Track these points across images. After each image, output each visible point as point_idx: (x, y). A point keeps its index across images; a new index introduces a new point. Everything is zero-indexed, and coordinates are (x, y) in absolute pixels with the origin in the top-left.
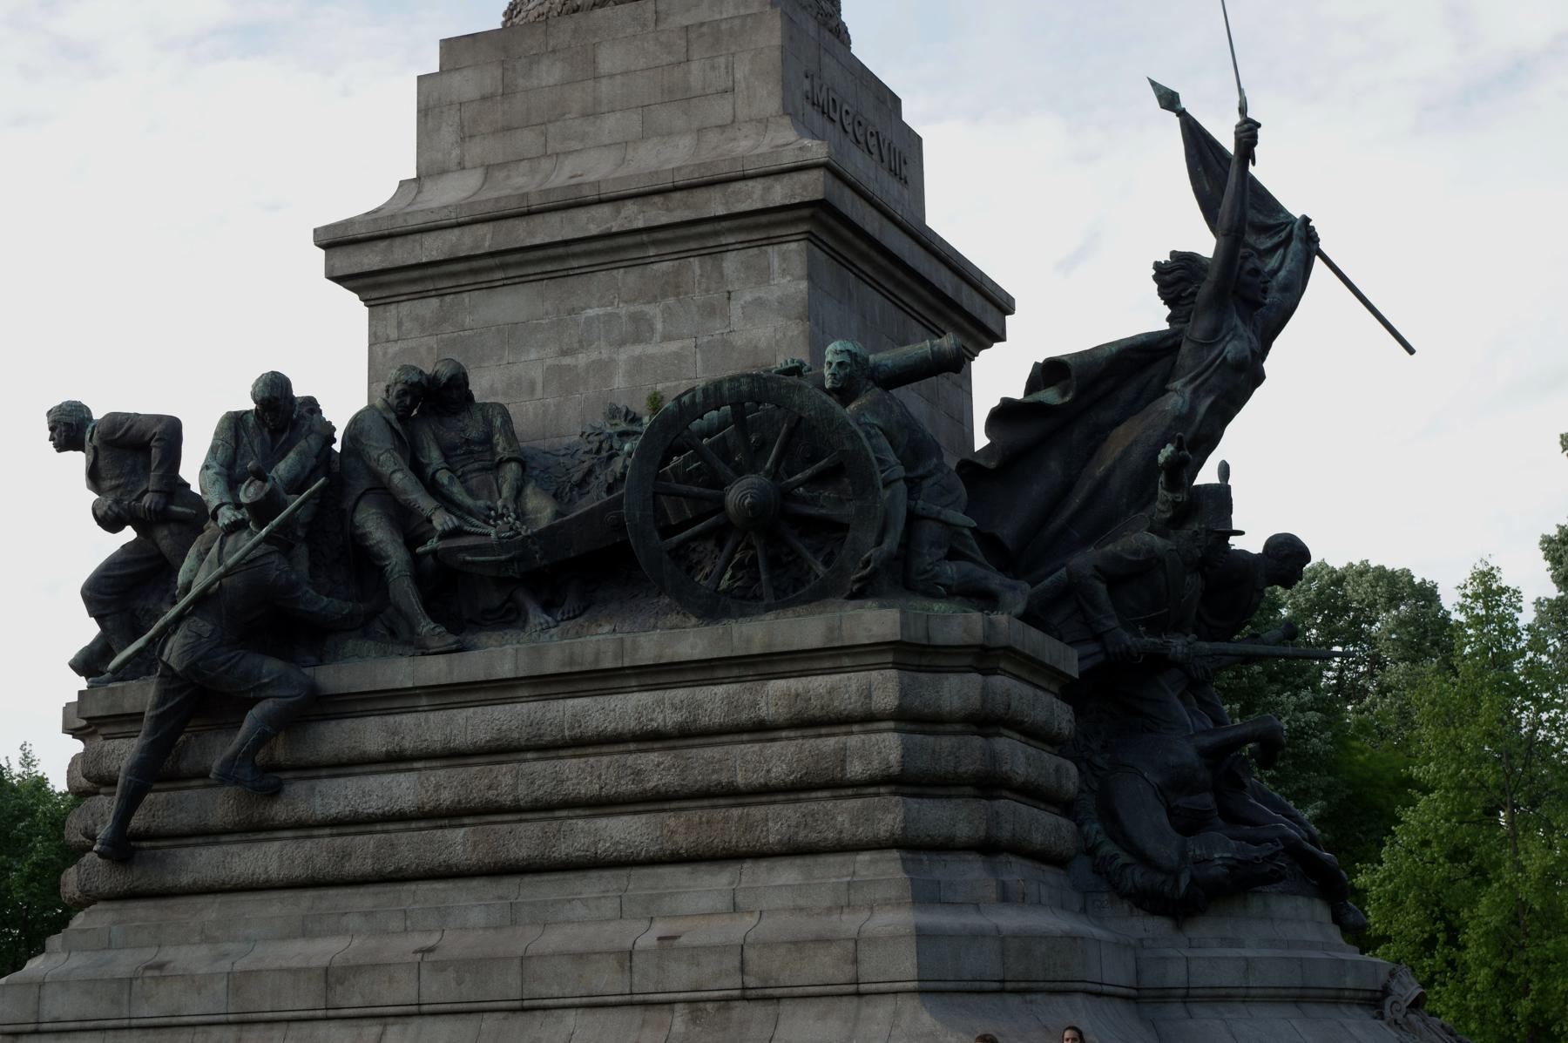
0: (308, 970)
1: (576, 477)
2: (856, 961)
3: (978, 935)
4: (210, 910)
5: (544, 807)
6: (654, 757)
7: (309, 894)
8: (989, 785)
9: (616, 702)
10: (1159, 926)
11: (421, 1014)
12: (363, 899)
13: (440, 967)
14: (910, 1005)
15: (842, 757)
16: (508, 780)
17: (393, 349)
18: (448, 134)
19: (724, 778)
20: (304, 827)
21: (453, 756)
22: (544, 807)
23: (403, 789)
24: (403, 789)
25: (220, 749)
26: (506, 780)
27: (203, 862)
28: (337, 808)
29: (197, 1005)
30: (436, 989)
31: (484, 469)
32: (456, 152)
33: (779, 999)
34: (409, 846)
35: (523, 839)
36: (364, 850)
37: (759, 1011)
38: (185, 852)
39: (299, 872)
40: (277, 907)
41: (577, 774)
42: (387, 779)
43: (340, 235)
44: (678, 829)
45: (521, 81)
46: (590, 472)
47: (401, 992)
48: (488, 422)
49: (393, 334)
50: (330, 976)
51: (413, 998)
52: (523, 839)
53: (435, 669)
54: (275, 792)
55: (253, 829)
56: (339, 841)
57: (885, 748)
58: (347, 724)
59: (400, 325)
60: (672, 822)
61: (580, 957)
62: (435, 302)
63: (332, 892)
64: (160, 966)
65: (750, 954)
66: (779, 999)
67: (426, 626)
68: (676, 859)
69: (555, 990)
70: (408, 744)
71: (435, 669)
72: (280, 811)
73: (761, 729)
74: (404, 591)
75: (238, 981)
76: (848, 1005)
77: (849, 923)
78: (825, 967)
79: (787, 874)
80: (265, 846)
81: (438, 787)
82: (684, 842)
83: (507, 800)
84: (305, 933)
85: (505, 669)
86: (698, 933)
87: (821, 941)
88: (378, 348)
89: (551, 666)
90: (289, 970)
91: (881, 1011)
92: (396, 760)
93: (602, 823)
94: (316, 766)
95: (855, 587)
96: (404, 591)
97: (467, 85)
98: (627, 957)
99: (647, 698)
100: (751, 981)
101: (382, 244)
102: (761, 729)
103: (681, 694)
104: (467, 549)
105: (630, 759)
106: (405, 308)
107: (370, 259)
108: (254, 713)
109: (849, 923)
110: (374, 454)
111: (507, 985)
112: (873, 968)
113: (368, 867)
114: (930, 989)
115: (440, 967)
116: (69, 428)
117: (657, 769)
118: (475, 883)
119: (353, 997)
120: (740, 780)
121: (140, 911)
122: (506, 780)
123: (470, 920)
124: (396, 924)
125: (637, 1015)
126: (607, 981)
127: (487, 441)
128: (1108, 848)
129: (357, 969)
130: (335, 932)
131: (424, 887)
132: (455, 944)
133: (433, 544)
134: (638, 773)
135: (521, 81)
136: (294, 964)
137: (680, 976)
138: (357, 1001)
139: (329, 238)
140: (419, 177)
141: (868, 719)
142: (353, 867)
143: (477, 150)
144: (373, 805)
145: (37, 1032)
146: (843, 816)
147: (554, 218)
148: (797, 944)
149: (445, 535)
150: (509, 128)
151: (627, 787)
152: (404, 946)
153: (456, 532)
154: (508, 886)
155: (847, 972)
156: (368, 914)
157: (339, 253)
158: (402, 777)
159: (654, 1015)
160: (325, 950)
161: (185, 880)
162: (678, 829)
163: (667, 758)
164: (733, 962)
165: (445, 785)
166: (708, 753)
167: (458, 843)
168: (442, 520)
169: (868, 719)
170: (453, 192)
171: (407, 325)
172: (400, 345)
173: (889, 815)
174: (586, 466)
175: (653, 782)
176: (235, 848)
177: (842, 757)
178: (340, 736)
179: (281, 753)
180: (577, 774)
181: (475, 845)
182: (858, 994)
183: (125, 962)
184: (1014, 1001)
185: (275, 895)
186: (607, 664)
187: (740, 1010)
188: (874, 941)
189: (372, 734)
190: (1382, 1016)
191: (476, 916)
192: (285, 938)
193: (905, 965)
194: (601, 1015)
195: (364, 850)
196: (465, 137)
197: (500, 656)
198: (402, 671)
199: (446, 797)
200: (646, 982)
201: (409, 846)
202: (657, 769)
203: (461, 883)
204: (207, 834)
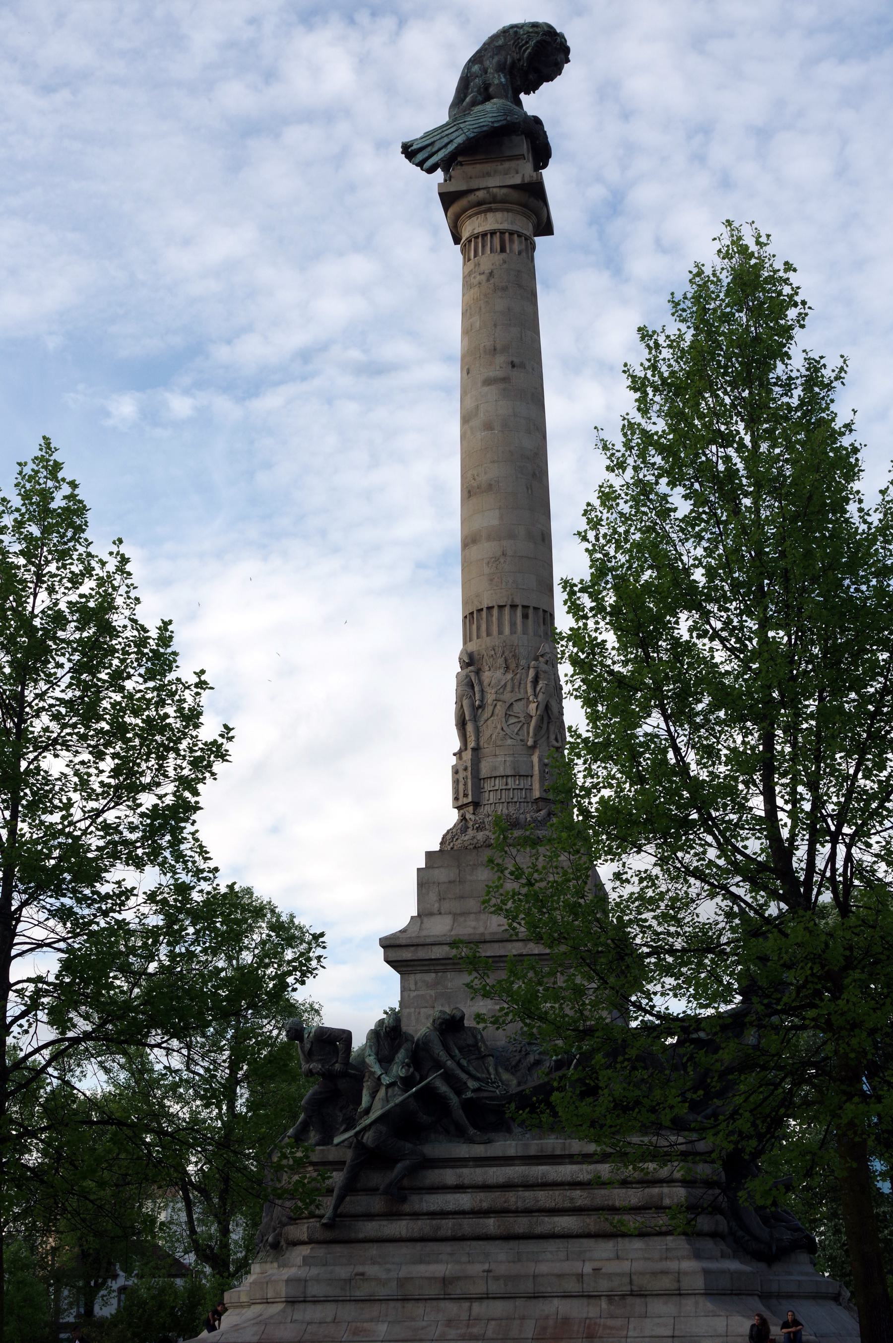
0: (435, 1278)
1: (514, 1063)
2: (679, 1281)
3: (723, 1272)
4: (373, 1250)
5: (528, 1212)
6: (578, 1192)
7: (419, 1246)
9: (561, 1168)
10: (762, 1266)
11: (488, 1298)
12: (447, 1247)
13: (497, 1278)
14: (701, 1299)
15: (661, 1197)
16: (513, 1199)
17: (413, 994)
18: (433, 896)
19: (610, 1203)
20: (416, 1215)
21: (485, 1187)
22: (528, 1212)
23: (465, 1201)
24: (465, 1201)
25: (379, 1179)
26: (513, 1199)
27: (370, 1228)
28: (433, 1208)
29: (382, 1292)
30: (495, 1288)
31: (477, 1059)
32: (437, 905)
33: (646, 1295)
34: (468, 1225)
35: (521, 1224)
36: (447, 1226)
37: (638, 1300)
38: (360, 1223)
39: (416, 1235)
40: (405, 1250)
41: (543, 1198)
42: (457, 1196)
43: (392, 942)
44: (591, 1223)
45: (469, 877)
46: (520, 1061)
47: (479, 1288)
48: (475, 1037)
49: (413, 987)
50: (445, 1281)
51: (485, 1290)
52: (521, 1224)
53: (479, 1150)
54: (404, 1200)
55: (392, 1215)
56: (434, 1222)
57: (679, 1193)
58: (437, 1171)
59: (416, 984)
60: (588, 1220)
61: (560, 1276)
62: (433, 975)
63: (430, 1244)
64: (362, 1274)
65: (634, 1277)
66: (646, 1295)
67: (472, 1131)
68: (589, 1236)
69: (549, 1290)
70: (466, 1182)
71: (479, 1150)
72: (406, 1208)
74: (459, 1114)
75: (402, 1282)
76: (675, 1299)
77: (673, 1265)
78: (666, 1283)
79: (638, 1244)
80: (399, 1223)
81: (481, 1201)
82: (593, 1228)
83: (513, 1208)
84: (421, 1262)
85: (511, 1152)
87: (664, 1272)
88: (406, 994)
89: (532, 1151)
90: (427, 1278)
91: (689, 1304)
92: (460, 1188)
93: (556, 1219)
94: (421, 1189)
96: (459, 1114)
97: (441, 875)
98: (580, 1277)
99: (575, 1167)
100: (635, 1288)
101: (412, 949)
103: (592, 1167)
104: (486, 1098)
105: (568, 1193)
106: (419, 976)
107: (407, 955)
108: (399, 1166)
109: (673, 1265)
110: (437, 1051)
111: (528, 1286)
112: (687, 1284)
113: (449, 1233)
114: (709, 1293)
115: (497, 1278)
117: (580, 1197)
118: (497, 1242)
119: (457, 1290)
120: (617, 1204)
121: (338, 1249)
122: (513, 1199)
123: (500, 1257)
124: (465, 1259)
125: (585, 1301)
126: (572, 1286)
127: (476, 1045)
128: (740, 1233)
129: (458, 1278)
130: (437, 1262)
131: (474, 1243)
132: (502, 1269)
133: (469, 1094)
134: (572, 1199)
135: (469, 877)
136: (427, 1275)
137: (604, 1285)
138: (459, 1292)
139: (388, 943)
140: (419, 915)
142: (441, 1233)
143: (446, 906)
144: (451, 1207)
145: (305, 1301)
146: (662, 1221)
147: (496, 945)
148: (654, 1274)
149: (474, 1091)
150: (462, 897)
151: (567, 1204)
152: (476, 1269)
153: (478, 1090)
154: (513, 1244)
155: (675, 1285)
156: (451, 1254)
157: (390, 950)
158: (463, 1195)
159: (592, 1301)
160: (438, 1269)
161: (361, 1236)
162: (591, 1223)
163: (585, 1194)
164: (626, 1280)
165: (484, 1200)
166: (603, 1192)
167: (491, 1224)
168: (472, 1084)
169: (669, 1181)
170: (440, 927)
171: (419, 984)
172: (415, 993)
174: (518, 1058)
175: (579, 1203)
176: (385, 1223)
177: (661, 1197)
178: (434, 1176)
179: (406, 1183)
180: (543, 1198)
181: (499, 1226)
182: (680, 1295)
183: (343, 1272)
184: (735, 1298)
185: (403, 1244)
186: (558, 1152)
187: (629, 1300)
188: (686, 1273)
189: (449, 1176)
190: (840, 1304)
191: (502, 1257)
192: (414, 1263)
193: (699, 1283)
194: (569, 1300)
195: (447, 1226)
196: (441, 899)
197: (507, 1146)
198: (463, 1150)
199: (485, 1205)
201: (468, 1225)
202: (580, 1197)
203: (491, 1242)
204: (370, 1216)
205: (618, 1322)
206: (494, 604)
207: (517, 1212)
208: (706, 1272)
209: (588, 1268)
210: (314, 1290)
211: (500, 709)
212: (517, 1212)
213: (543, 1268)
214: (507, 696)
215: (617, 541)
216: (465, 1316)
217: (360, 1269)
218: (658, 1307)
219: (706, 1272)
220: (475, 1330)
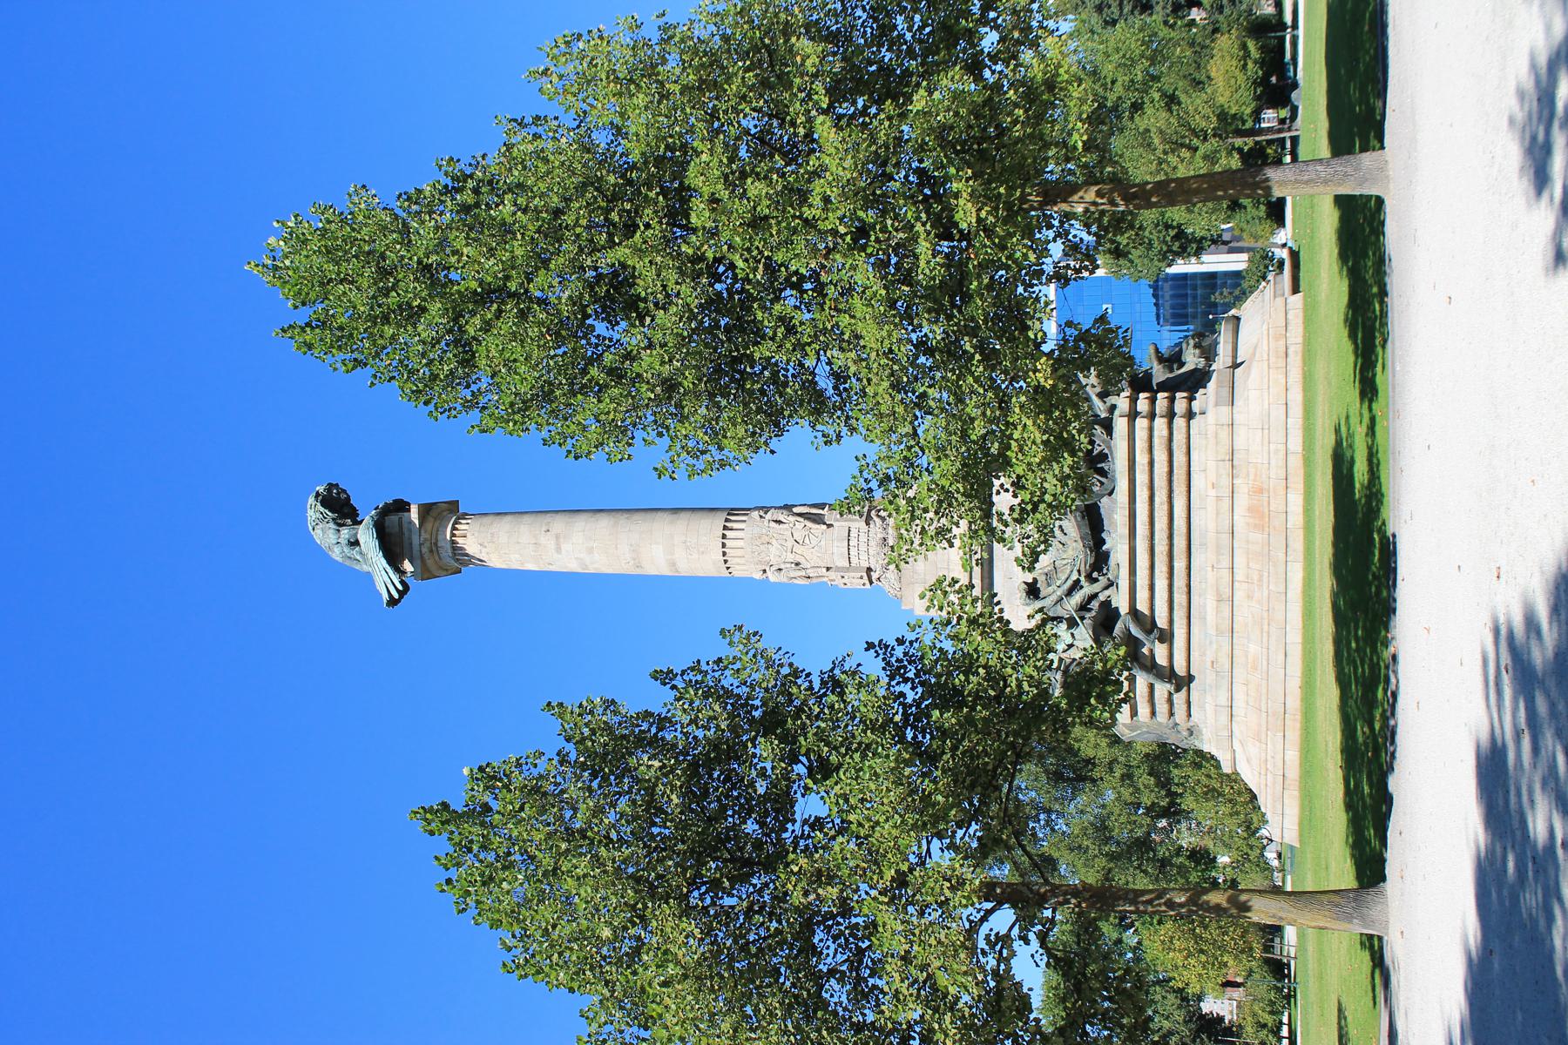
5: (1171, 537)
8: (1171, 415)
13: (1218, 561)
20: (1171, 621)
29: (1226, 648)
30: (1226, 563)
47: (1226, 574)
57: (1160, 424)
73: (1151, 463)
75: (1219, 632)
77: (1211, 429)
78: (1224, 434)
82: (1184, 489)
86: (1212, 477)
91: (1238, 418)
95: (1145, 650)
102: (1151, 463)
111: (1226, 538)
113: (1185, 596)
115: (1218, 561)
116: (656, 675)
126: (1226, 503)
137: (1225, 481)
141: (1151, 429)
142: (1185, 603)
146: (1179, 437)
152: (1211, 575)
160: (1211, 604)
167: (1179, 565)
169: (1151, 429)
173: (1179, 422)
200: (1227, 492)
201: (1179, 582)
205: (1252, 470)
206: (721, 532)
207: (1171, 546)
208: (1217, 404)
209: (1212, 493)
210: (1223, 699)
211: (798, 548)
212: (1171, 546)
213: (1212, 526)
214: (790, 543)
215: (744, 948)
216: (1245, 586)
217: (1209, 664)
218: (1240, 443)
219: (1217, 404)
220: (1256, 578)
